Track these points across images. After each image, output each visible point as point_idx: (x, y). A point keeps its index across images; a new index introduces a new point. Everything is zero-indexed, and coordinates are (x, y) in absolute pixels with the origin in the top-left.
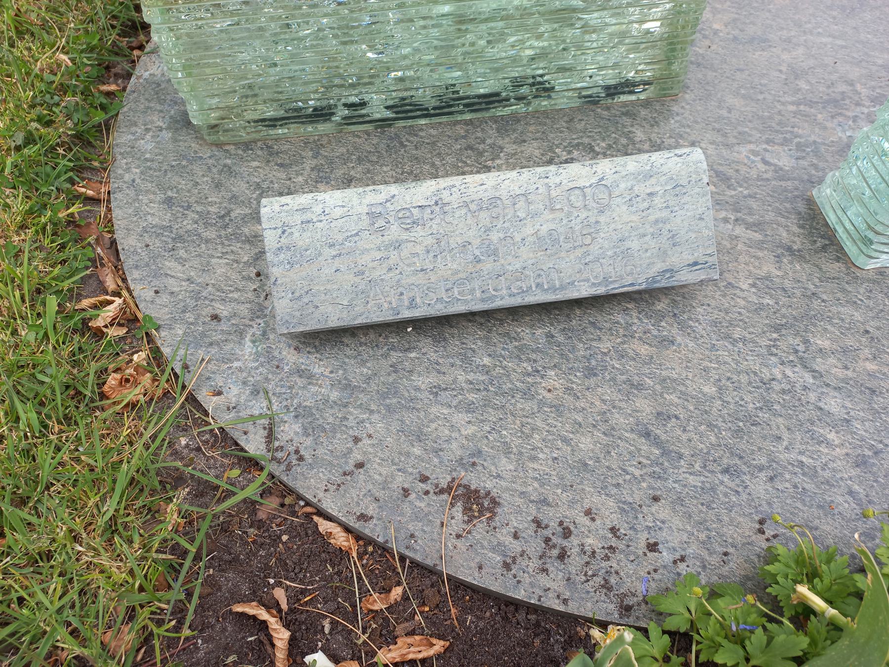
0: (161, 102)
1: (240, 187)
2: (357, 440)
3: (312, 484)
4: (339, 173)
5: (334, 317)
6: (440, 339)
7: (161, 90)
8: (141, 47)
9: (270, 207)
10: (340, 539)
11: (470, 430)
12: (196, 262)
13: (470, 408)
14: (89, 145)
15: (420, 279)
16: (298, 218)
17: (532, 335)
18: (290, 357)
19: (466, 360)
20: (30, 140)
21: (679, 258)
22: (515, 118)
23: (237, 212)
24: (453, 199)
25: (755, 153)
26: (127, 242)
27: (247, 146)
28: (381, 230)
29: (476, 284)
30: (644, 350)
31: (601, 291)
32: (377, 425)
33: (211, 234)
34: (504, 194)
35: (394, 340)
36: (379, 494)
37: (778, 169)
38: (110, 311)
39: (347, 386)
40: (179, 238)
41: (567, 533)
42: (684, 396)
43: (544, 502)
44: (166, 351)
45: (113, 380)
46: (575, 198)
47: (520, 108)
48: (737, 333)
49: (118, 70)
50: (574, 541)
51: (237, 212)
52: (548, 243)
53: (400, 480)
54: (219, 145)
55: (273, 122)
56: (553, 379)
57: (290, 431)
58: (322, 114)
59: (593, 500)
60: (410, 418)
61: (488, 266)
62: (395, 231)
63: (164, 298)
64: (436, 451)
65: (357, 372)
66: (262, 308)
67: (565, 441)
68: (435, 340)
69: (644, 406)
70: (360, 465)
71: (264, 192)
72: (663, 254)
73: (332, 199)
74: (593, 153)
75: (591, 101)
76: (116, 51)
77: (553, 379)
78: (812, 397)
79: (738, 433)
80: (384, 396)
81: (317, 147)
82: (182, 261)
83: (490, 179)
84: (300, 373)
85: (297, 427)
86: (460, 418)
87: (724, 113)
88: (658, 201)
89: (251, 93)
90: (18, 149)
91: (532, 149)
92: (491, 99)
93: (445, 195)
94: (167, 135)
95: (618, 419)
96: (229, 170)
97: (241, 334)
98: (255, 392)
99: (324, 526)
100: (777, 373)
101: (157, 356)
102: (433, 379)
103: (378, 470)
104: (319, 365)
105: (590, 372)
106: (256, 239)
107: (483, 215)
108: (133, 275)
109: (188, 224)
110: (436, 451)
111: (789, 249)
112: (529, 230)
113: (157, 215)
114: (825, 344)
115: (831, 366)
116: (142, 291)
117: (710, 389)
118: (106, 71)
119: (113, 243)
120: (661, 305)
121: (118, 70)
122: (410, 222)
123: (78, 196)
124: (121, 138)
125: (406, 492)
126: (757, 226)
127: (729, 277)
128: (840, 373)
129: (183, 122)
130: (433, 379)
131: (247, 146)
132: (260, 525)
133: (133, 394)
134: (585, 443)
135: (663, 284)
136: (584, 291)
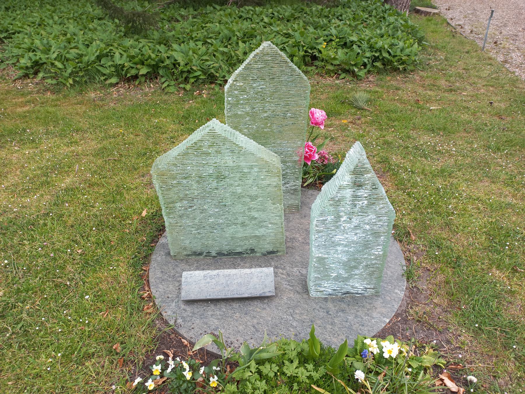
0: (164, 249)
1: (179, 269)
2: (193, 324)
3: (182, 331)
4: (202, 268)
5: (193, 297)
6: (216, 305)
7: (165, 246)
8: (161, 235)
9: (184, 274)
10: (186, 342)
11: (217, 323)
12: (166, 286)
13: (218, 319)
14: (147, 258)
15: (212, 290)
16: (189, 276)
17: (236, 305)
18: (183, 306)
19: (220, 309)
20: (136, 257)
21: (266, 290)
22: (245, 258)
23: (177, 275)
24: (221, 274)
25: (298, 270)
26: (151, 280)
27: (182, 260)
28: (206, 279)
29: (224, 292)
30: (259, 310)
31: (250, 296)
32: (198, 321)
33: (170, 279)
34: (231, 274)
35: (205, 304)
36: (196, 334)
37: (302, 274)
38: (146, 295)
39: (194, 313)
40: (163, 280)
41: (232, 344)
42: (264, 320)
43: (229, 338)
44: (157, 303)
45: (146, 308)
46: (246, 275)
47: (247, 255)
48: (280, 308)
49: (155, 241)
50: (233, 345)
51: (177, 275)
52: (240, 284)
53: (201, 332)
54: (175, 260)
55: (189, 255)
56: (238, 315)
57: (180, 321)
58: (200, 254)
59: (239, 338)
60: (205, 320)
61: (227, 288)
62: (208, 280)
63: (158, 293)
64: (209, 327)
65: (196, 310)
66: (178, 296)
67: (237, 327)
68: (215, 305)
69: (255, 321)
70: (193, 328)
71: (184, 270)
72: (263, 289)
73: (197, 272)
74: (261, 267)
75: (264, 255)
76: (156, 236)
77: (238, 315)
78: (291, 322)
79: (272, 328)
80: (201, 316)
81: (198, 261)
82: (163, 285)
83: (229, 271)
84: (184, 310)
85: (181, 320)
86: (215, 321)
87: (294, 260)
88: (263, 277)
89: (185, 249)
90: (133, 258)
91: (247, 265)
92: (240, 253)
93: (220, 273)
94: (164, 257)
95: (249, 323)
96: (177, 266)
97: (173, 301)
98: (174, 313)
99: (183, 340)
100: (285, 317)
101: (154, 304)
102: (212, 313)
103: (196, 329)
104: (189, 308)
105: (246, 314)
106: (180, 281)
107: (227, 278)
108: (152, 287)
109: (165, 277)
110: (209, 327)
111: (298, 292)
112: (236, 281)
113: (159, 275)
114: (297, 312)
115: (297, 317)
116: (153, 290)
117: (270, 319)
118: (153, 241)
119: (148, 281)
120: (266, 301)
121: (155, 241)
122: (211, 278)
123: (143, 270)
124: (153, 257)
125: (201, 334)
126: (292, 286)
127: (282, 296)
128: (298, 318)
129: (169, 254)
130: (212, 313)
131: (182, 260)
132: (170, 339)
133: (149, 311)
134: (241, 328)
135: (263, 295)
136: (246, 295)
